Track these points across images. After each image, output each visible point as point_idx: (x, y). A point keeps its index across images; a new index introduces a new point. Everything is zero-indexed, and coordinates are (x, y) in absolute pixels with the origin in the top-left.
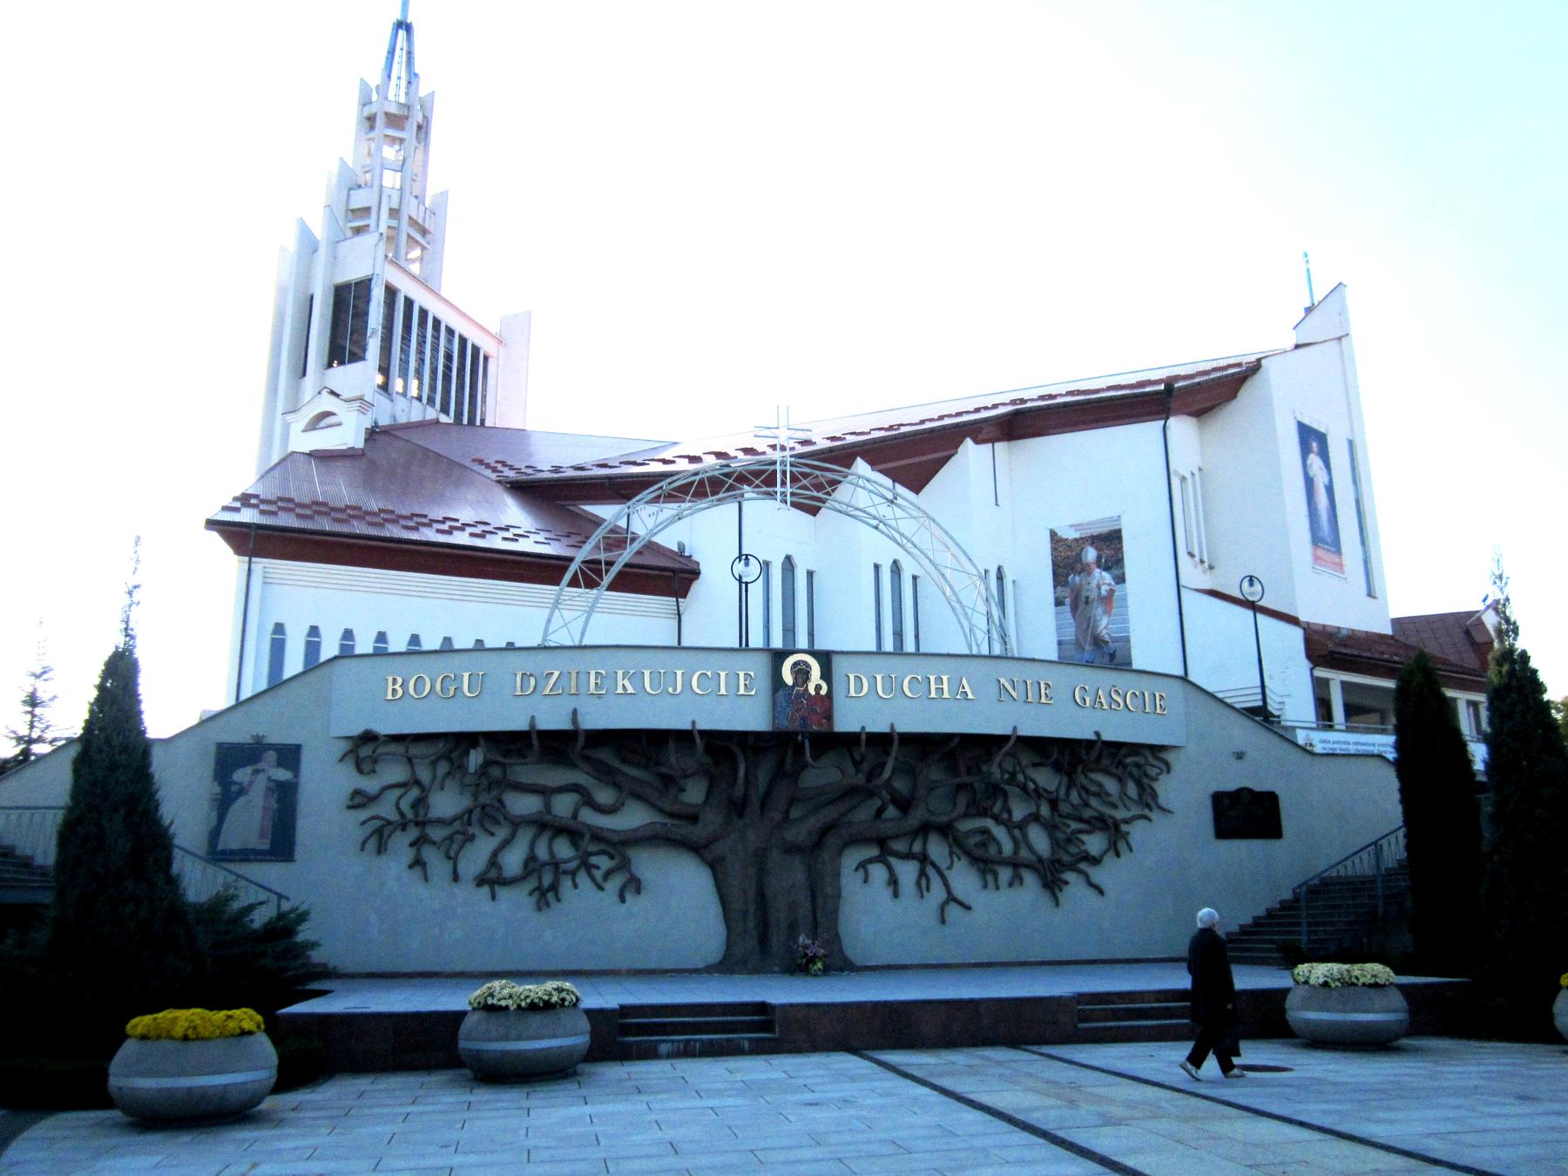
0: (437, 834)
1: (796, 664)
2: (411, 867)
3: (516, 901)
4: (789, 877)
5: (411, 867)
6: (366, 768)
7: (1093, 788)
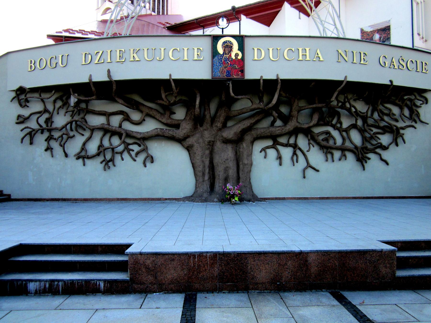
0: (56, 135)
1: (224, 43)
2: (46, 150)
3: (95, 166)
4: (225, 155)
5: (46, 150)
7: (386, 112)
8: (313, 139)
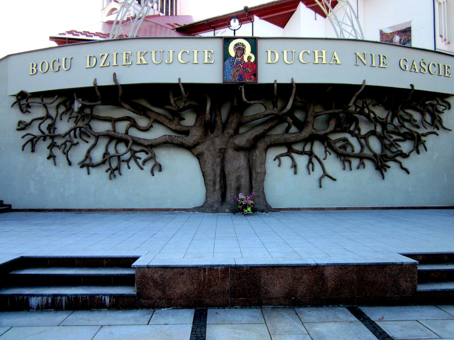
0: (59, 142)
1: (236, 45)
2: (48, 158)
3: (100, 175)
4: (237, 163)
5: (48, 158)
7: (407, 117)
8: (329, 146)
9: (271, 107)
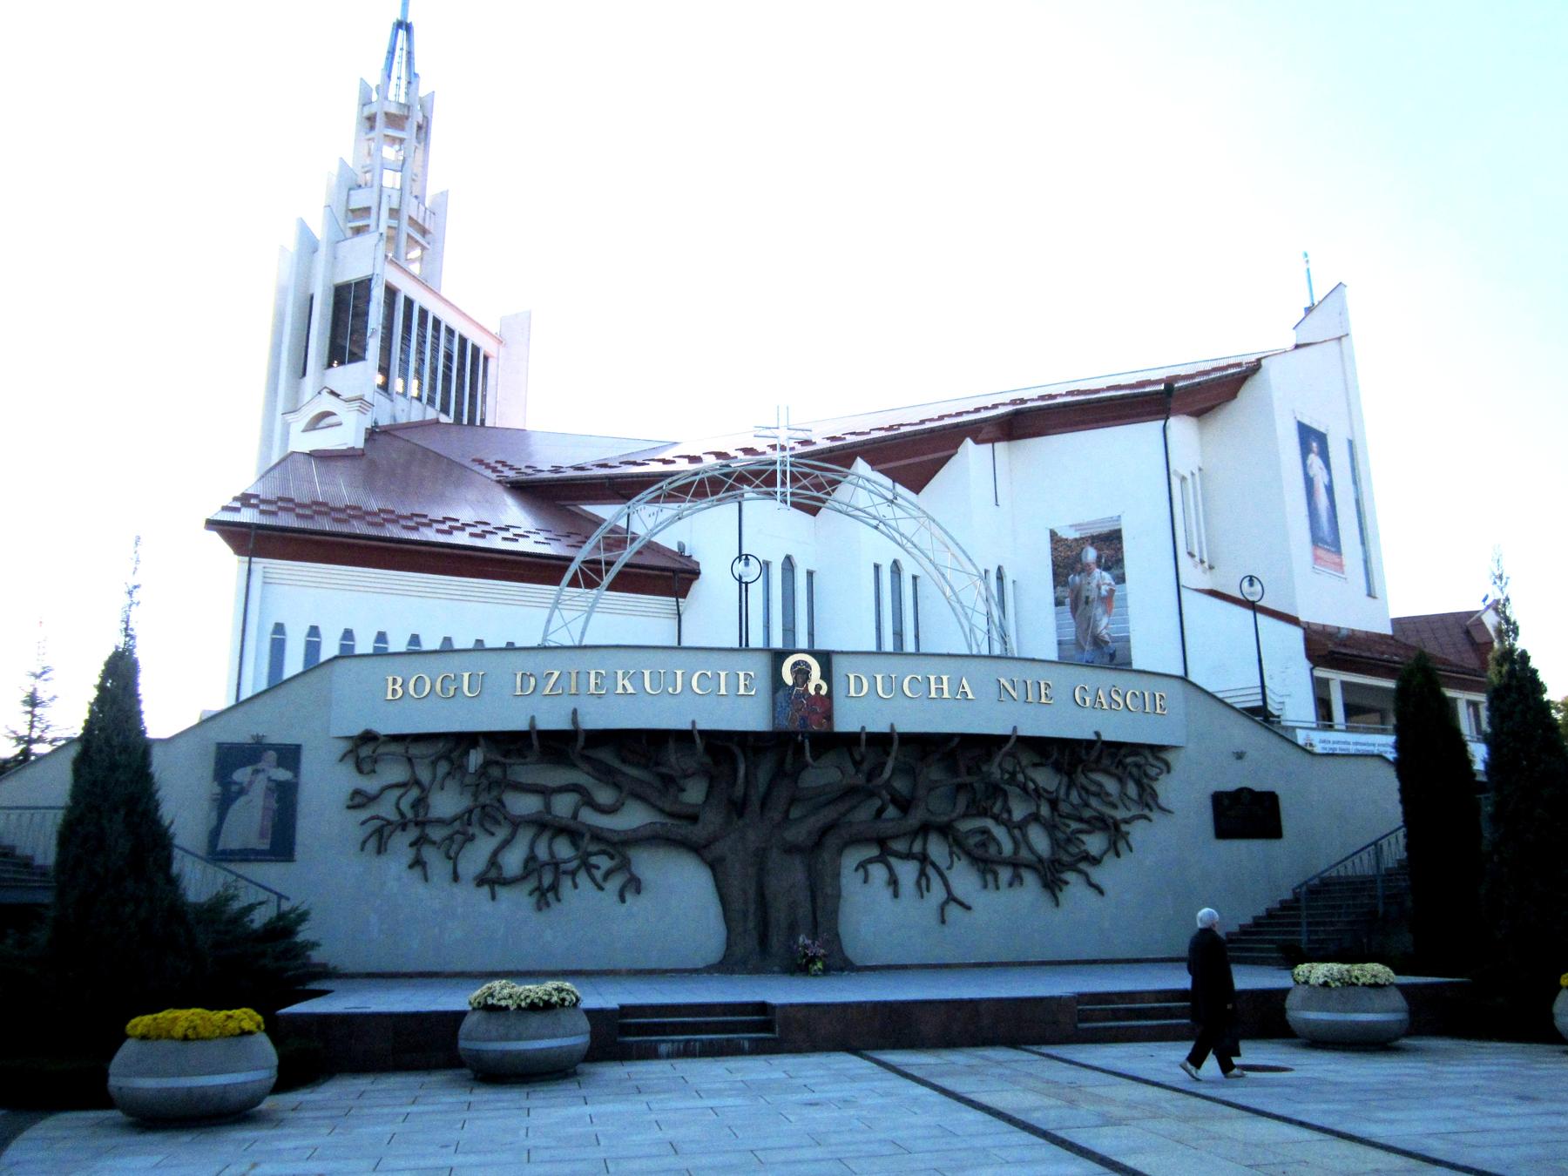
0: (437, 834)
1: (796, 664)
2: (411, 867)
3: (516, 901)
4: (789, 877)
5: (411, 867)
6: (366, 768)
7: (1093, 788)
9: (851, 769)
